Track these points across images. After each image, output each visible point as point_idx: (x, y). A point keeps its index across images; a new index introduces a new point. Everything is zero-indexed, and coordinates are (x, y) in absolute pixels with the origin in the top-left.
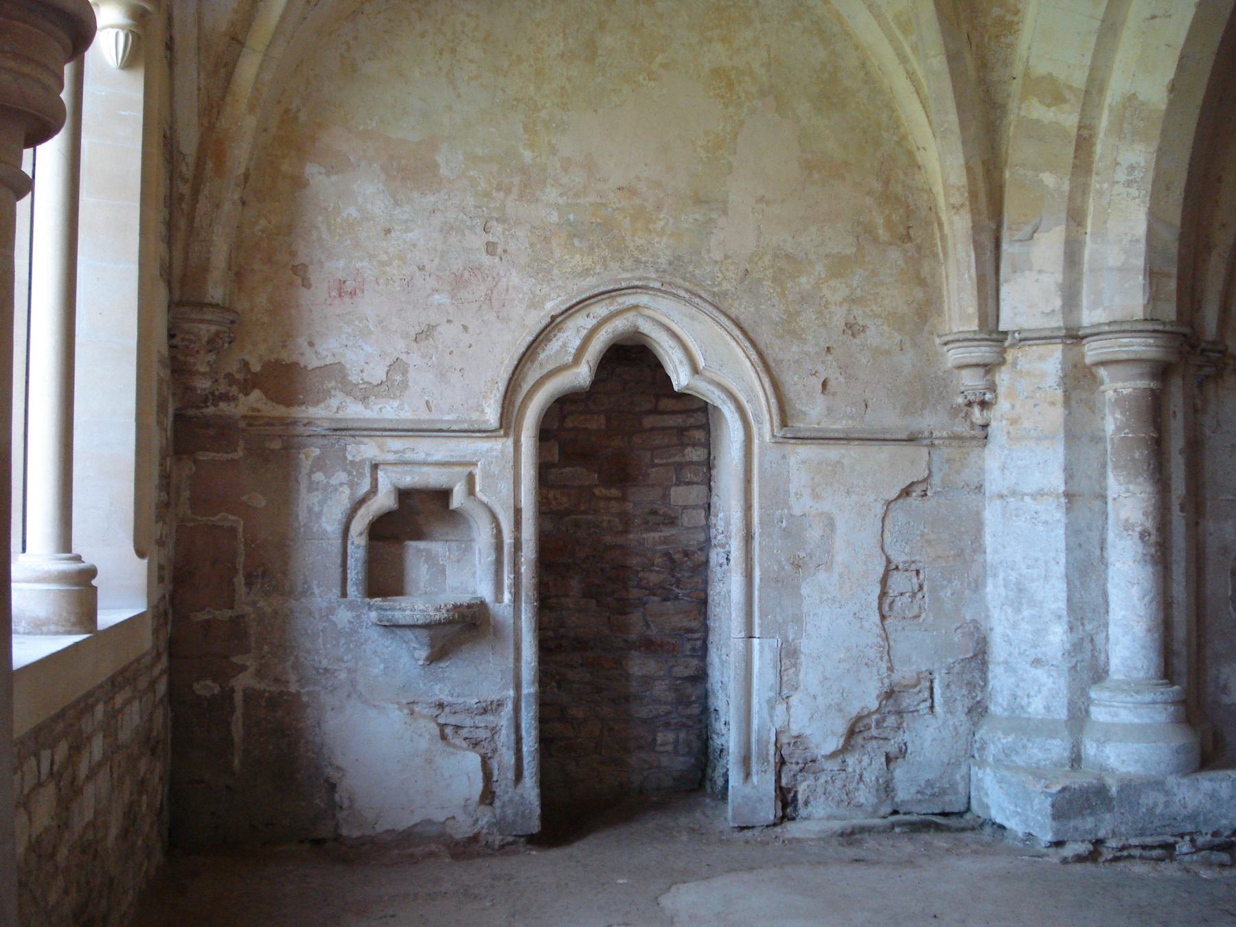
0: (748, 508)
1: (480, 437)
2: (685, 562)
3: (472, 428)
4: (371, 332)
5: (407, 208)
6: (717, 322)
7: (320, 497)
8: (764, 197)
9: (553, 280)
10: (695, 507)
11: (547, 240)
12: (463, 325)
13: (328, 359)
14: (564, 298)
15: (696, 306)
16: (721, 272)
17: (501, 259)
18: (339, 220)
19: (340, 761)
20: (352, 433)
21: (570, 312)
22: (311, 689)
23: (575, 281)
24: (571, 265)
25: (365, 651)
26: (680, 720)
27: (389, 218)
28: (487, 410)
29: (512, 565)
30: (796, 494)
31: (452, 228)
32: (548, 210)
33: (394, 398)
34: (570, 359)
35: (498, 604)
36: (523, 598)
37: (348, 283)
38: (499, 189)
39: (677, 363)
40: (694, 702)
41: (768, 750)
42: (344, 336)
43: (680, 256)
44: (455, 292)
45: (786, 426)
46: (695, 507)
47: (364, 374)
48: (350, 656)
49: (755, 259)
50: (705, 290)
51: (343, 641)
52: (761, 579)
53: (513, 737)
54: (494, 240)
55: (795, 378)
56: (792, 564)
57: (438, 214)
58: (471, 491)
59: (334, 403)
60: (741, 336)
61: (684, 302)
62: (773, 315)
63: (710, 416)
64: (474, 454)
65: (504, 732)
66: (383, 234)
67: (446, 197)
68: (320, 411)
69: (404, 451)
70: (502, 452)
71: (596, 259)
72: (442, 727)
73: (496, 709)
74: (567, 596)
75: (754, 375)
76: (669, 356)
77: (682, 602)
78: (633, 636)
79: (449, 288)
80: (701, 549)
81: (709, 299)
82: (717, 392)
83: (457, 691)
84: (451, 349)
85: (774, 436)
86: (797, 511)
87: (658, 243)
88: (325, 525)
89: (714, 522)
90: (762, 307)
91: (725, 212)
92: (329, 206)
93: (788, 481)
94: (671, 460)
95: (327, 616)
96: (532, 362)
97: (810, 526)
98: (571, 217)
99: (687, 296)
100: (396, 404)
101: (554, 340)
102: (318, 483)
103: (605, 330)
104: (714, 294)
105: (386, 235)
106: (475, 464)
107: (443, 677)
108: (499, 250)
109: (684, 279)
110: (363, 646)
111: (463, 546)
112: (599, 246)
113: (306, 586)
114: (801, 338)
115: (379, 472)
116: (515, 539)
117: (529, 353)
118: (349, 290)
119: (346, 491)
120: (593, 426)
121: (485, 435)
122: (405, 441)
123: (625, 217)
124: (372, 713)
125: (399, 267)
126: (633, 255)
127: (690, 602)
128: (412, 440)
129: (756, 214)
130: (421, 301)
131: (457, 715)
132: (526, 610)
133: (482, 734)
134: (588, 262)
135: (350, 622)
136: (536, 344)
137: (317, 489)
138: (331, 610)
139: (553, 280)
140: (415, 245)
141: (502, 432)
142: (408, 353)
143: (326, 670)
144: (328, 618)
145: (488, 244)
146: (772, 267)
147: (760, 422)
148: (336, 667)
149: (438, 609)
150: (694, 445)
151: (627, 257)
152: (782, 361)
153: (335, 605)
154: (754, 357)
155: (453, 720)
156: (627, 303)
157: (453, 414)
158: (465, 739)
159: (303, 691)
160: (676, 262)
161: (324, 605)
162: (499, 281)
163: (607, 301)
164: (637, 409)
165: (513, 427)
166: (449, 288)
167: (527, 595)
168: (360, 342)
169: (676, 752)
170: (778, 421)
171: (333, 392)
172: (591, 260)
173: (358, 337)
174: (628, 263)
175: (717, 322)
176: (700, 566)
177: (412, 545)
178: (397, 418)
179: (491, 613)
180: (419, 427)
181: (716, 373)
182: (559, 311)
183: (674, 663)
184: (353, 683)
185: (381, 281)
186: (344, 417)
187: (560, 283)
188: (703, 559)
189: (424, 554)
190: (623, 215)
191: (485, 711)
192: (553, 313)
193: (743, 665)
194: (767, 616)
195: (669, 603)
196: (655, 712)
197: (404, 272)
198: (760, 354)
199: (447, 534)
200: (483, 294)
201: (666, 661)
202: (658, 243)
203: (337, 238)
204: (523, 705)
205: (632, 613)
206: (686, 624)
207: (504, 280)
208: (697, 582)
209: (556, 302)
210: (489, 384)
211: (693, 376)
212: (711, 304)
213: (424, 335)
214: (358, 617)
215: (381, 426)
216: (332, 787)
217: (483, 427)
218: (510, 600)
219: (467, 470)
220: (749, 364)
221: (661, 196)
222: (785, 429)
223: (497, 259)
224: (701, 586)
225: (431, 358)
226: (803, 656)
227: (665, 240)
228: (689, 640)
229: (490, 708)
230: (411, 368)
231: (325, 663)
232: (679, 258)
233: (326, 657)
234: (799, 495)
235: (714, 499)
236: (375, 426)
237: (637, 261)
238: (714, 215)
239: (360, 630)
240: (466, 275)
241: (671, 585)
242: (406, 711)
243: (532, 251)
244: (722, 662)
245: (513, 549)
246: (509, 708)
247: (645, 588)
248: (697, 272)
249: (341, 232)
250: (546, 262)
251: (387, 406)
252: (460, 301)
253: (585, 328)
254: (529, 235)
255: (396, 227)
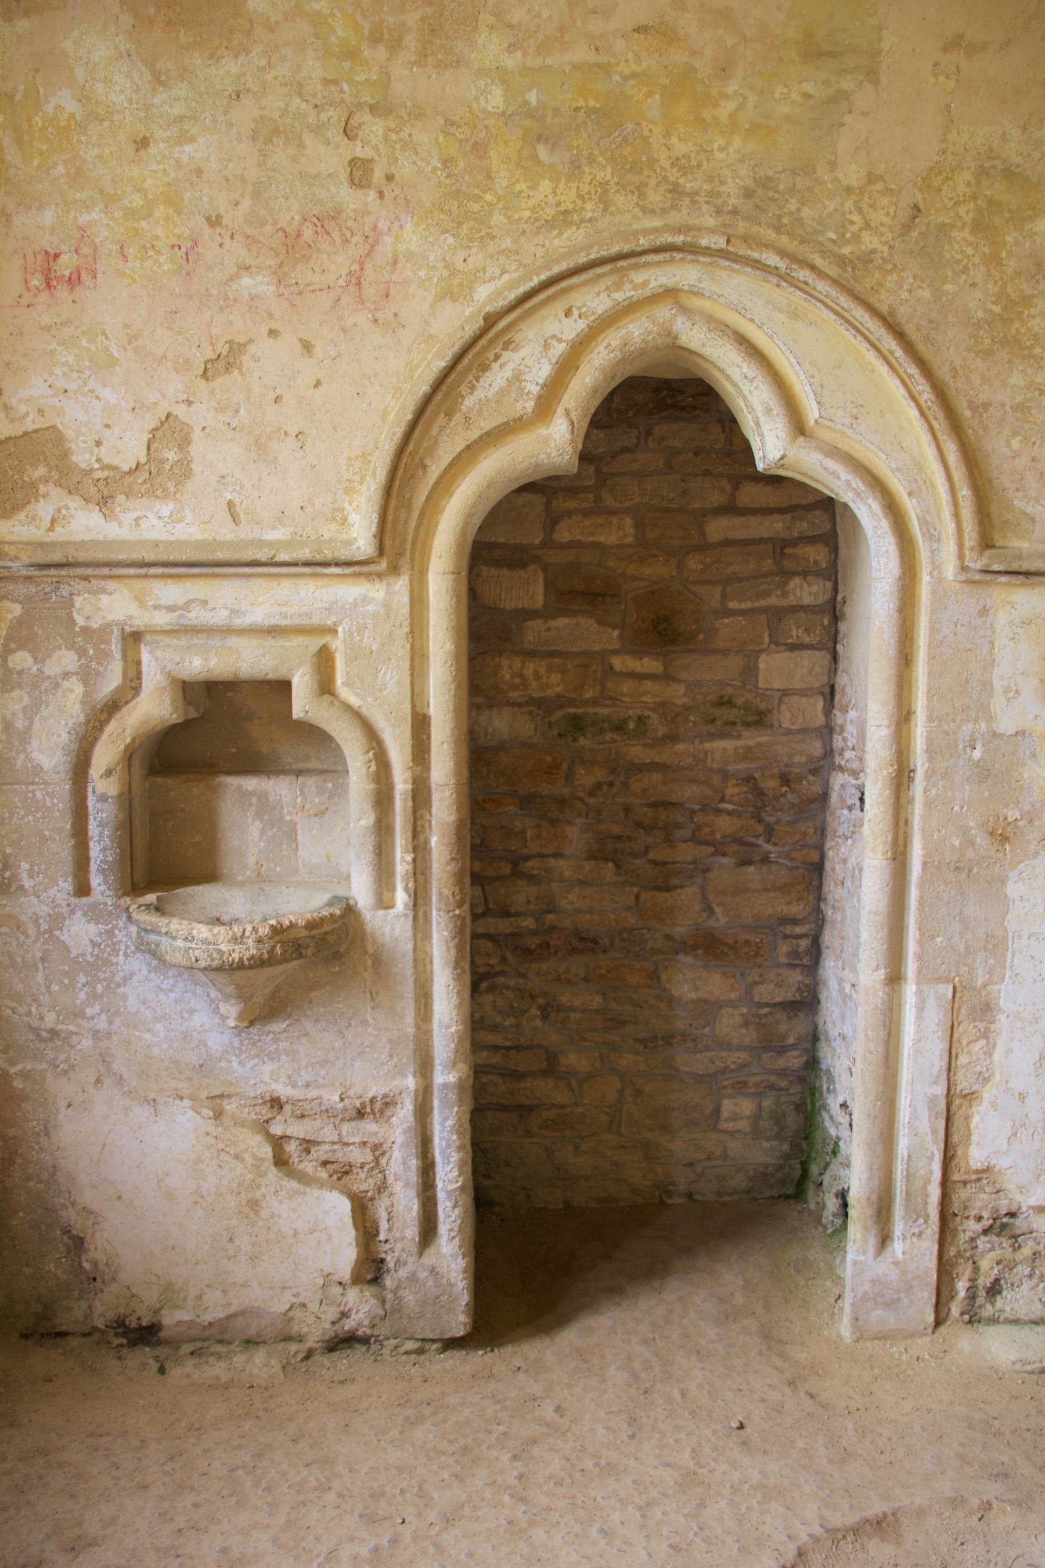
0: (903, 717)
1: (338, 575)
2: (784, 795)
3: (319, 558)
4: (112, 362)
5: (181, 90)
6: (847, 321)
7: (26, 700)
8: (961, 36)
9: (493, 238)
10: (804, 693)
11: (480, 149)
12: (301, 340)
13: (29, 419)
14: (515, 275)
15: (803, 287)
16: (860, 211)
17: (381, 195)
18: (38, 120)
19: (88, 1198)
20: (79, 571)
21: (527, 305)
22: (29, 1067)
23: (540, 239)
24: (532, 202)
25: (125, 997)
26: (764, 1077)
27: (142, 114)
28: (355, 518)
29: (410, 834)
30: (1007, 690)
31: (276, 131)
32: (481, 83)
33: (166, 496)
34: (530, 405)
35: (381, 912)
36: (434, 899)
37: (64, 259)
38: (375, 39)
39: (760, 414)
40: (793, 1047)
41: (927, 1196)
42: (58, 371)
43: (770, 179)
44: (286, 269)
45: (993, 547)
46: (804, 693)
47: (103, 449)
48: (97, 1008)
49: (936, 182)
50: (823, 254)
51: (82, 979)
52: (924, 864)
53: (414, 1163)
54: (368, 153)
55: (1016, 443)
56: (991, 834)
57: (246, 101)
58: (325, 687)
59: (44, 509)
60: (899, 353)
61: (775, 280)
62: (972, 305)
63: (838, 519)
64: (329, 610)
65: (397, 1154)
66: (130, 151)
67: (264, 63)
68: (18, 529)
69: (187, 606)
70: (387, 605)
71: (585, 188)
72: (278, 1143)
73: (382, 1112)
74: (558, 855)
75: (925, 438)
76: (745, 399)
77: (774, 867)
78: (680, 929)
79: (273, 263)
80: (815, 772)
81: (833, 271)
82: (845, 474)
83: (306, 1076)
84: (278, 392)
85: (964, 568)
86: (1006, 725)
87: (722, 149)
88: (36, 755)
89: (839, 721)
90: (949, 287)
91: (872, 76)
92: (15, 89)
93: (990, 664)
94: (763, 603)
95: (50, 931)
96: (449, 415)
97: (1034, 755)
98: (533, 97)
99: (782, 265)
100: (166, 509)
101: (495, 366)
102: (20, 673)
103: (605, 344)
104: (843, 262)
105: (137, 150)
106: (333, 631)
107: (277, 1050)
108: (378, 174)
109: (778, 229)
110: (122, 990)
111: (330, 785)
112: (591, 159)
113: (7, 874)
114: (1029, 356)
115: (142, 646)
116: (414, 783)
117: (439, 396)
118: (67, 273)
119: (77, 688)
120: (609, 538)
121: (349, 570)
122: (188, 584)
123: (650, 94)
124: (141, 1113)
125: (167, 218)
126: (665, 178)
127: (791, 869)
128: (201, 582)
129: (942, 78)
130: (215, 292)
131: (306, 1120)
132: (439, 923)
133: (357, 1156)
134: (568, 196)
135: (94, 944)
136: (453, 376)
137: (20, 686)
138: (57, 921)
139: (493, 238)
140: (199, 172)
141: (384, 565)
142: (189, 403)
143: (54, 1033)
144: (52, 935)
145: (353, 162)
146: (974, 197)
147: (934, 538)
148: (72, 1028)
149: (238, 940)
150: (805, 574)
151: (652, 183)
152: (986, 406)
153: (64, 910)
154: (926, 395)
155: (298, 1130)
156: (653, 284)
157: (283, 529)
158: (325, 1163)
159: (13, 1070)
160: (760, 191)
161: (44, 910)
162: (376, 242)
163: (608, 281)
164: (697, 505)
165: (408, 554)
166: (273, 263)
167: (440, 894)
168: (92, 383)
169: (756, 1132)
170: (975, 536)
171: (42, 489)
172: (574, 190)
173: (87, 372)
174: (655, 197)
175: (847, 321)
176: (811, 801)
177: (232, 781)
178: (172, 538)
179: (369, 928)
180: (210, 557)
181: (843, 433)
182: (501, 303)
183: (758, 979)
184: (105, 1058)
185: (131, 251)
186: (65, 539)
187: (507, 243)
188: (817, 789)
189: (254, 800)
190: (646, 89)
191: (360, 1114)
192: (489, 308)
193: (882, 1034)
194: (933, 938)
195: (751, 869)
196: (720, 1064)
197: (177, 231)
198: (940, 393)
199: (307, 757)
200: (344, 272)
201: (743, 975)
202: (722, 149)
203: (36, 162)
204: (436, 1103)
205: (682, 887)
206: (783, 908)
207: (388, 240)
208: (805, 834)
209: (499, 283)
210: (358, 464)
211: (794, 439)
212: (835, 282)
213: (222, 364)
214: (110, 933)
215: (135, 556)
216: (78, 1244)
217: (343, 554)
218: (406, 905)
219: (314, 644)
220: (914, 413)
221: (730, 42)
222: (987, 553)
223: (372, 195)
224: (812, 840)
225: (237, 412)
226: (1002, 1017)
227: (737, 142)
228: (786, 937)
229: (368, 1110)
230: (196, 435)
231: (50, 1019)
232: (766, 183)
233: (52, 1008)
234: (1013, 693)
235: (842, 680)
236: (123, 556)
237: (676, 190)
238: (847, 84)
239: (114, 960)
240: (308, 234)
241: (757, 836)
242: (207, 1112)
243: (449, 176)
244: (845, 998)
245: (410, 804)
246: (405, 1113)
247: (707, 843)
248: (806, 212)
249: (44, 148)
250: (478, 198)
251: (149, 514)
252: (295, 289)
253: (560, 341)
254: (441, 139)
255: (159, 134)
